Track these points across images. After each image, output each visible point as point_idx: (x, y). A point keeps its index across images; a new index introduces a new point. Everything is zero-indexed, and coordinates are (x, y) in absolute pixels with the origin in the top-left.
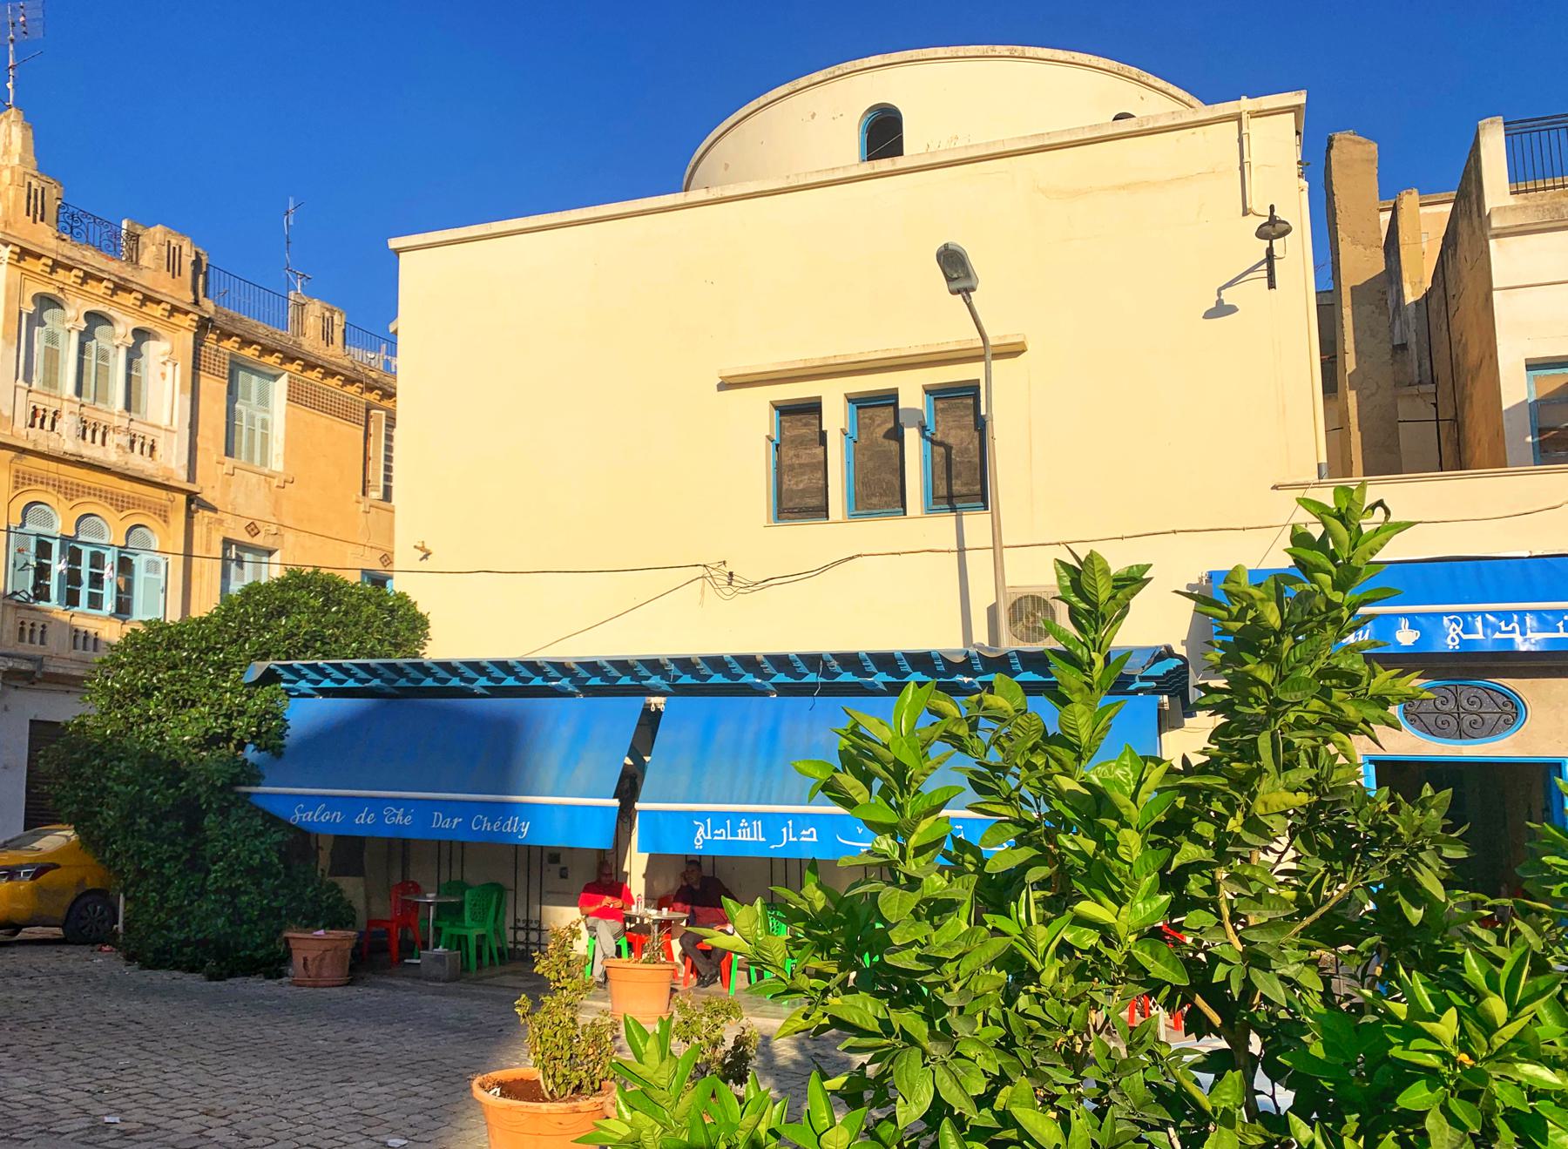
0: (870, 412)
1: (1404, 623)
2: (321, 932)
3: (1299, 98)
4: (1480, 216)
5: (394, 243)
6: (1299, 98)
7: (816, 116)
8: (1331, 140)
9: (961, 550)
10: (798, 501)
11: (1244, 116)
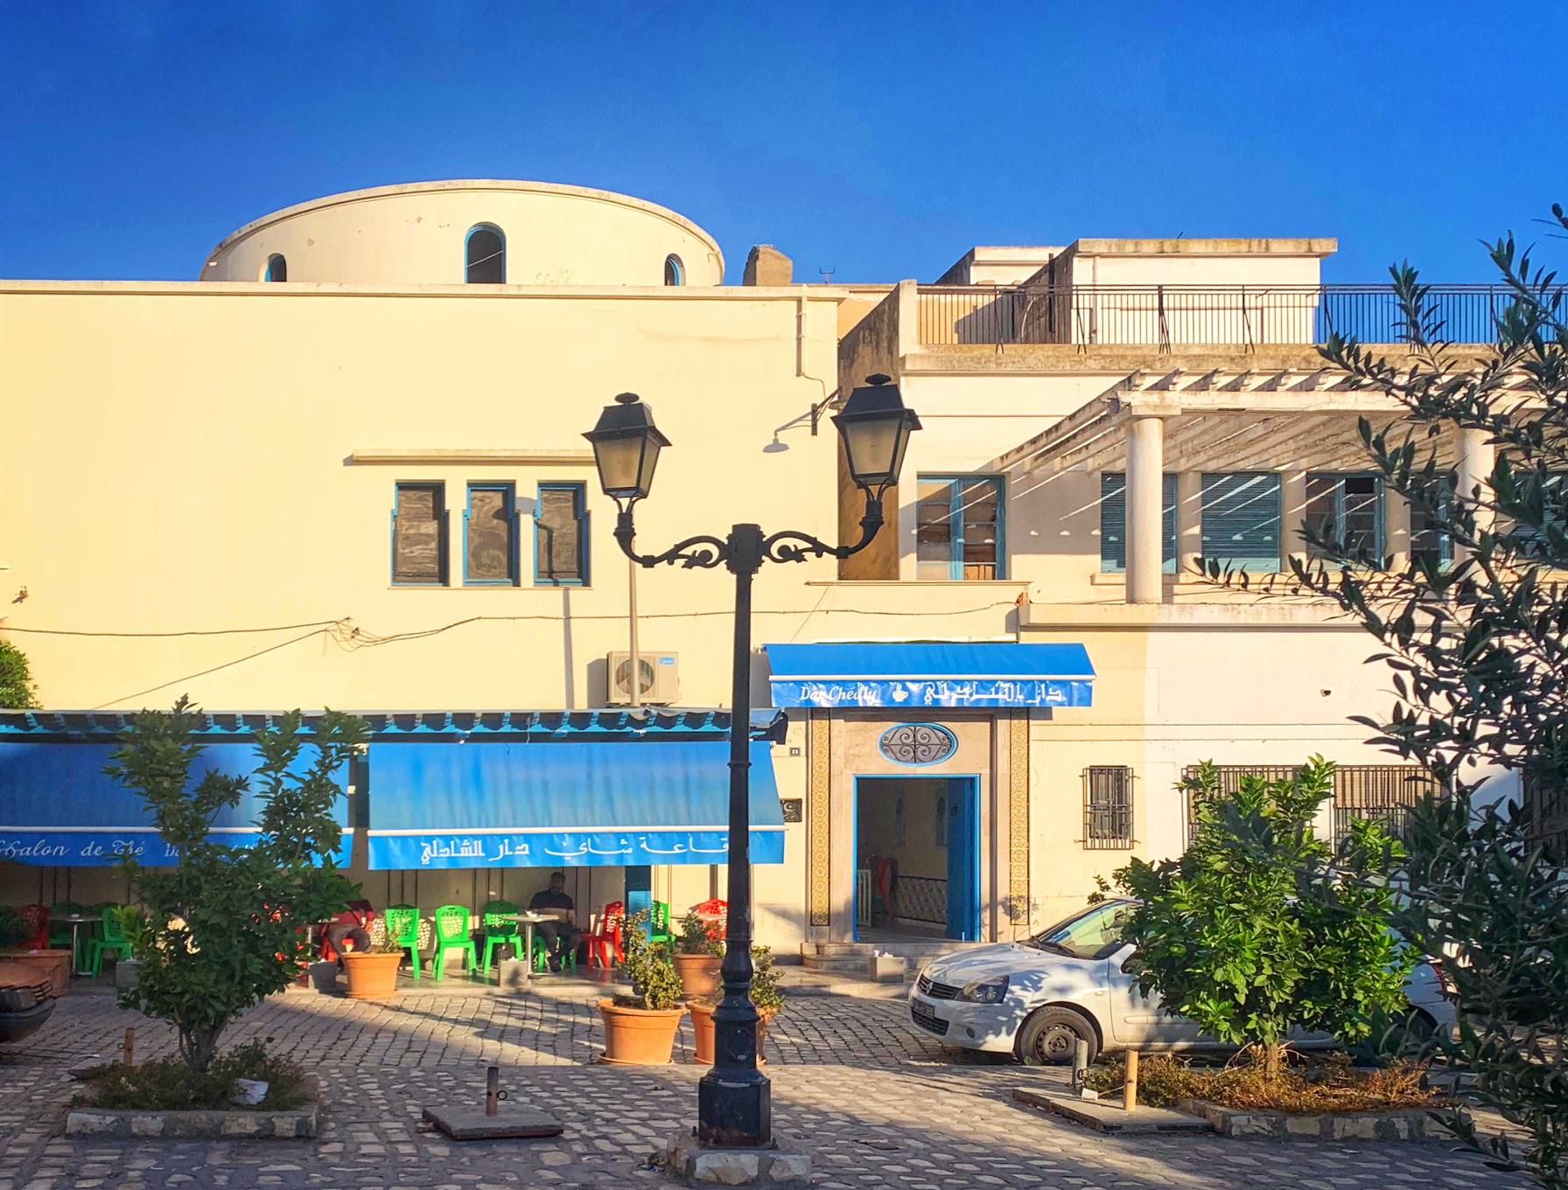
0: (479, 494)
1: (899, 686)
2: (35, 952)
4: (890, 352)
7: (421, 223)
8: (754, 256)
10: (421, 565)
11: (804, 300)
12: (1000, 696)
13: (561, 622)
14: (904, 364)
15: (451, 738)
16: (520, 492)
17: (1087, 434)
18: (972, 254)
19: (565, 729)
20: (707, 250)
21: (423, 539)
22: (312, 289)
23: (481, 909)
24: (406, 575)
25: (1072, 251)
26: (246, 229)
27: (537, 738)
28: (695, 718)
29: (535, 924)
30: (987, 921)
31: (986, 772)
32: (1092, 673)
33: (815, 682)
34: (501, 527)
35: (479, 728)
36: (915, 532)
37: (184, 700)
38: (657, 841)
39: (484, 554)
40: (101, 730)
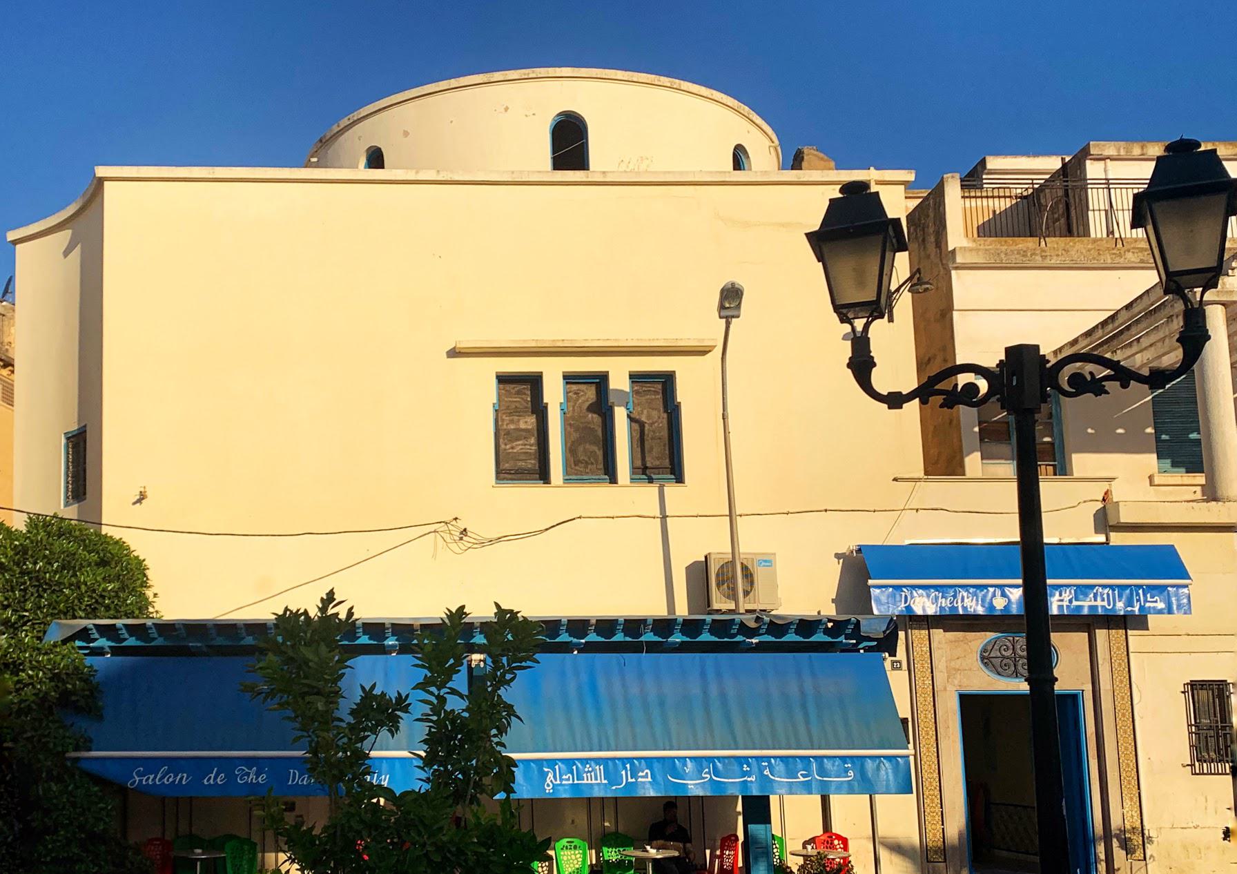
0: (574, 387)
1: (998, 592)
3: (910, 176)
5: (101, 171)
7: (509, 110)
9: (664, 517)
10: (522, 463)
12: (1099, 603)
13: (739, 510)
14: (954, 258)
15: (565, 648)
16: (614, 384)
17: (1141, 326)
18: (983, 162)
19: (677, 638)
20: (768, 143)
21: (521, 434)
22: (411, 176)
23: (598, 841)
24: (508, 472)
25: (1083, 155)
26: (345, 122)
27: (652, 648)
28: (806, 626)
29: (655, 861)
30: (1102, 856)
31: (1088, 688)
32: (1186, 576)
33: (914, 587)
34: (595, 419)
35: (593, 637)
36: (977, 429)
37: (330, 597)
38: (780, 767)
39: (581, 449)
40: (220, 641)
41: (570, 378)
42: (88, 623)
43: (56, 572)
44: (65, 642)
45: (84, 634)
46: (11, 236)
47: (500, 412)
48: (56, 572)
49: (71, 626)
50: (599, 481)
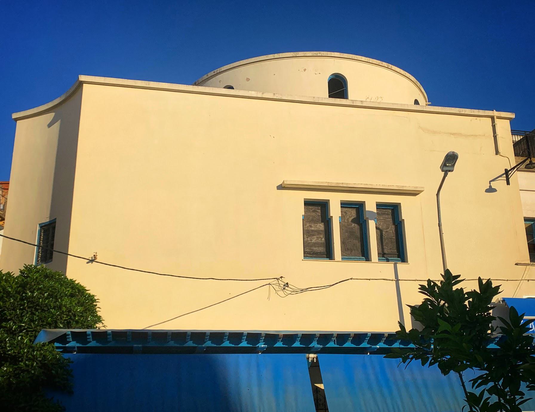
3: (513, 116)
5: (82, 78)
6: (513, 116)
7: (313, 69)
10: (318, 248)
15: (363, 351)
22: (260, 95)
34: (355, 226)
41: (344, 205)
42: (68, 331)
43: (47, 298)
44: (50, 342)
45: (63, 339)
46: (14, 116)
47: (306, 220)
48: (47, 298)
49: (55, 333)
50: (359, 260)
